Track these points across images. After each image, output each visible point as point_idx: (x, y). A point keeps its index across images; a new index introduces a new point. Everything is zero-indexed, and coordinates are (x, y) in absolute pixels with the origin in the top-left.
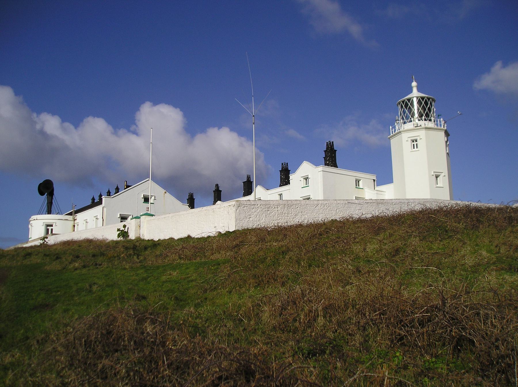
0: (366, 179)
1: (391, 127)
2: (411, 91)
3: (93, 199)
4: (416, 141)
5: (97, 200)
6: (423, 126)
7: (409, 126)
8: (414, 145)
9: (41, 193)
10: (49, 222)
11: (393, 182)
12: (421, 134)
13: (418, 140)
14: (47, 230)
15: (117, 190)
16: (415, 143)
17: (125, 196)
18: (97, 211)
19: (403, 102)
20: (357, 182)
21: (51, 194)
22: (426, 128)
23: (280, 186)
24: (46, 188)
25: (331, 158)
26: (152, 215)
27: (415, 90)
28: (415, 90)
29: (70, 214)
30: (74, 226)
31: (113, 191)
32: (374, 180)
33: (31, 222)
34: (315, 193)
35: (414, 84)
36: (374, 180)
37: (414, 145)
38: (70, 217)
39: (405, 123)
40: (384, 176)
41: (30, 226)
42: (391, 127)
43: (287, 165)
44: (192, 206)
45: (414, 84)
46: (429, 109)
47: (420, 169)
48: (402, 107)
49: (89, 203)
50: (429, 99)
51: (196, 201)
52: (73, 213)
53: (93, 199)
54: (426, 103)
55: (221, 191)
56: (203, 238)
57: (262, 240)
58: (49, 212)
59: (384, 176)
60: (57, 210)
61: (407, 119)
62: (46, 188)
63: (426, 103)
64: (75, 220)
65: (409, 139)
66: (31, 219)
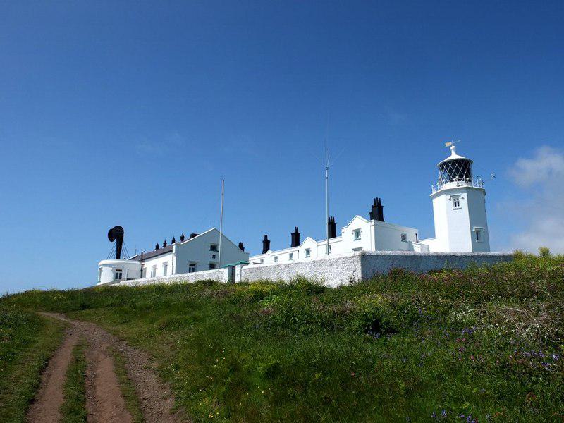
3: (157, 247)
24: (116, 235)
27: (453, 153)
28: (453, 153)
58: (118, 257)
62: (116, 235)
66: (99, 264)
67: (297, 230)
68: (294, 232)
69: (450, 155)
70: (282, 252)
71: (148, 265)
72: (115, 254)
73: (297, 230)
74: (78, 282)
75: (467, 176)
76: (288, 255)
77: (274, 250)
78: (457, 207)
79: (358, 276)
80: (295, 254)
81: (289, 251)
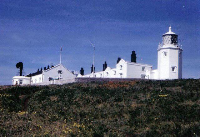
3: (38, 70)
5: (40, 70)
14: (20, 82)
15: (49, 68)
18: (40, 76)
20: (143, 68)
22: (171, 48)
24: (20, 66)
25: (134, 59)
27: (170, 30)
28: (170, 30)
32: (151, 68)
36: (151, 68)
38: (29, 78)
45: (170, 28)
47: (165, 66)
49: (37, 71)
53: (38, 70)
56: (132, 57)
58: (21, 75)
59: (155, 66)
62: (20, 66)
65: (163, 52)
66: (13, 78)
67: (106, 62)
68: (104, 63)
69: (168, 31)
70: (137, 64)
71: (33, 78)
72: (19, 74)
73: (106, 62)
74: (172, 47)
75: (175, 43)
76: (141, 68)
77: (141, 62)
78: (166, 56)
79: (178, 79)
80: (103, 74)
81: (101, 73)
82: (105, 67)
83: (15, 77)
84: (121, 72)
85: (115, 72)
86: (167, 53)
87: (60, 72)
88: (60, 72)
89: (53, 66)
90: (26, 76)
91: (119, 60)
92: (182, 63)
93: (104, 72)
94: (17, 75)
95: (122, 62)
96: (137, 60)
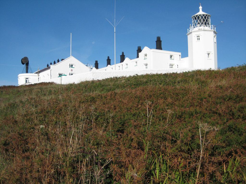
0: (177, 55)
1: (188, 29)
2: (199, 11)
4: (199, 37)
6: (203, 29)
7: (196, 29)
8: (198, 38)
9: (23, 64)
10: (27, 77)
11: (188, 56)
12: (201, 33)
13: (200, 36)
16: (199, 38)
17: (61, 63)
19: (194, 17)
20: (171, 56)
21: (27, 64)
23: (121, 62)
24: (25, 62)
26: (66, 75)
27: (201, 10)
28: (201, 10)
29: (37, 73)
30: (39, 78)
31: (56, 61)
32: (180, 55)
33: (19, 77)
34: (153, 62)
35: (201, 7)
37: (198, 38)
38: (37, 74)
39: (195, 27)
40: (185, 54)
41: (18, 79)
42: (188, 29)
43: (140, 47)
44: (97, 66)
45: (201, 7)
46: (207, 21)
47: (201, 51)
48: (193, 19)
50: (207, 15)
51: (163, 44)
52: (38, 73)
54: (205, 17)
55: (110, 60)
57: (186, 81)
58: (27, 72)
59: (185, 54)
60: (30, 71)
61: (196, 25)
62: (25, 62)
63: (205, 17)
64: (39, 76)
65: (196, 36)
66: (18, 76)
67: (123, 53)
73: (123, 53)
75: (205, 24)
82: (122, 59)
83: (20, 75)
84: (145, 63)
85: (136, 62)
86: (27, 78)
87: (71, 66)
88: (71, 66)
89: (62, 60)
90: (35, 73)
91: (139, 50)
92: (42, 70)
93: (122, 63)
94: (23, 73)
95: (146, 50)
96: (162, 46)
